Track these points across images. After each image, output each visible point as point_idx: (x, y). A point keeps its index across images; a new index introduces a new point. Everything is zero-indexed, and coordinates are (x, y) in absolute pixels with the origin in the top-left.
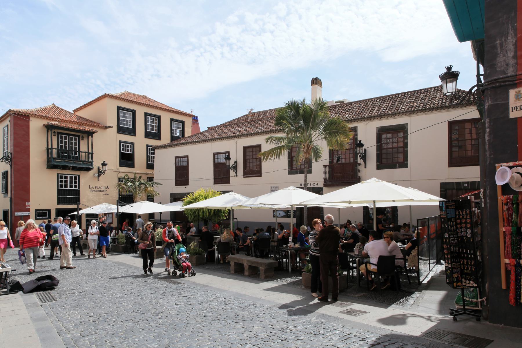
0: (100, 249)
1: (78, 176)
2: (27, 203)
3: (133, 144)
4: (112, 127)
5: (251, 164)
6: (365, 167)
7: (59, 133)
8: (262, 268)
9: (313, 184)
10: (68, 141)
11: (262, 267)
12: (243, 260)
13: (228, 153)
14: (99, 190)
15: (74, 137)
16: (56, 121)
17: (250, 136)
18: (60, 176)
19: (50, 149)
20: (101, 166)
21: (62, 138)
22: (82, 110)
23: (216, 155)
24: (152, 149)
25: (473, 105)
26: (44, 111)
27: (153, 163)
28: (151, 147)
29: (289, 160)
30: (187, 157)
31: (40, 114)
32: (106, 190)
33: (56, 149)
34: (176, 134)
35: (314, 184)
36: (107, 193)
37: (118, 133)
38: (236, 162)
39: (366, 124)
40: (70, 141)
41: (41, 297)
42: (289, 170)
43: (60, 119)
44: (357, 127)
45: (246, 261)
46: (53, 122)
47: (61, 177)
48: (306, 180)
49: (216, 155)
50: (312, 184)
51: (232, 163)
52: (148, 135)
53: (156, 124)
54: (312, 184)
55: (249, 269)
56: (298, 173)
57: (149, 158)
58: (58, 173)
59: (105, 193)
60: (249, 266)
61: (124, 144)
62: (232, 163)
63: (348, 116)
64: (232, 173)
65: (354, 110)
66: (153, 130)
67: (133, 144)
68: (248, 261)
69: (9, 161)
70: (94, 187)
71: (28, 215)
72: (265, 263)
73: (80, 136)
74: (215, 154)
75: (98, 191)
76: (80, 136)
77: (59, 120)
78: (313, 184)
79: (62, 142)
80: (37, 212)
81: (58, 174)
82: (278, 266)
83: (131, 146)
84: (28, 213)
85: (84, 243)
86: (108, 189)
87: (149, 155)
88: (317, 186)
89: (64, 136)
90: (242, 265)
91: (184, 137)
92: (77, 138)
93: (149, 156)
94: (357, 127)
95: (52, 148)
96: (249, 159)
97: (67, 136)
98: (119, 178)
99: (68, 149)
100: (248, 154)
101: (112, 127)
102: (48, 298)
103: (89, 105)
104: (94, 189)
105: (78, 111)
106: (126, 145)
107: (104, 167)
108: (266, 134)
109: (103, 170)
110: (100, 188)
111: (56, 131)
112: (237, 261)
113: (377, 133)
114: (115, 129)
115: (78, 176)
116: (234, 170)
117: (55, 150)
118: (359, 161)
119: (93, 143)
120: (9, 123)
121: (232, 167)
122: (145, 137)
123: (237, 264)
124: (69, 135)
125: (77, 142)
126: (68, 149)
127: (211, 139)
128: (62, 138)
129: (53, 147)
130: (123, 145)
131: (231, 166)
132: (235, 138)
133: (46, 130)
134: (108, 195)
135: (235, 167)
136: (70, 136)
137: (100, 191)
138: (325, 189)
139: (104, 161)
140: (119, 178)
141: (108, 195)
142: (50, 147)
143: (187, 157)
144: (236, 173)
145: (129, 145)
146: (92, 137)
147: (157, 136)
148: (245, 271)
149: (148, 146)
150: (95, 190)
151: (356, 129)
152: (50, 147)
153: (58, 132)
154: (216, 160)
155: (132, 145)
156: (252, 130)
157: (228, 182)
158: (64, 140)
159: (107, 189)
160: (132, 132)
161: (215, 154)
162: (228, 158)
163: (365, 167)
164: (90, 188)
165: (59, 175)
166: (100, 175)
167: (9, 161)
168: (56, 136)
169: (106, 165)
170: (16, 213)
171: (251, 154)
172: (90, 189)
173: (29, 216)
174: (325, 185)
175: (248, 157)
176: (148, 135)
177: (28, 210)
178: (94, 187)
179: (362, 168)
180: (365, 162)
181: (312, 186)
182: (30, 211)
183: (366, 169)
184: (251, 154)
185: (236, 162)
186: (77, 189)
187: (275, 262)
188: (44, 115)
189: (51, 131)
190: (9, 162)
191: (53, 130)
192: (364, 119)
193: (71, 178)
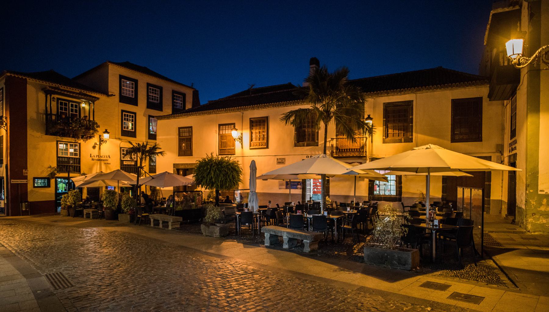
2: (24, 170)
3: (135, 114)
4: (115, 95)
7: (58, 99)
12: (281, 232)
15: (74, 104)
19: (49, 114)
25: (474, 85)
30: (191, 127)
32: (107, 159)
34: (128, 128)
41: (52, 280)
42: (296, 142)
45: (285, 233)
53: (158, 94)
55: (288, 242)
60: (289, 238)
61: (126, 113)
66: (127, 115)
67: (135, 114)
68: (288, 233)
69: (4, 125)
70: (95, 156)
71: (25, 182)
79: (61, 109)
80: (266, 118)
82: (119, 214)
84: (25, 180)
85: (87, 212)
89: (64, 102)
97: (67, 102)
98: (121, 148)
99: (68, 116)
101: (115, 95)
102: (62, 282)
106: (125, 114)
113: (384, 109)
120: (4, 86)
123: (155, 220)
124: (69, 101)
126: (68, 116)
130: (125, 115)
136: (70, 103)
140: (121, 148)
143: (191, 127)
145: (131, 115)
153: (57, 98)
155: (134, 115)
160: (134, 101)
164: (91, 157)
165: (122, 149)
166: (102, 144)
167: (4, 125)
172: (91, 158)
173: (27, 184)
177: (26, 178)
178: (95, 156)
186: (78, 157)
189: (51, 96)
190: (4, 127)
191: (53, 96)
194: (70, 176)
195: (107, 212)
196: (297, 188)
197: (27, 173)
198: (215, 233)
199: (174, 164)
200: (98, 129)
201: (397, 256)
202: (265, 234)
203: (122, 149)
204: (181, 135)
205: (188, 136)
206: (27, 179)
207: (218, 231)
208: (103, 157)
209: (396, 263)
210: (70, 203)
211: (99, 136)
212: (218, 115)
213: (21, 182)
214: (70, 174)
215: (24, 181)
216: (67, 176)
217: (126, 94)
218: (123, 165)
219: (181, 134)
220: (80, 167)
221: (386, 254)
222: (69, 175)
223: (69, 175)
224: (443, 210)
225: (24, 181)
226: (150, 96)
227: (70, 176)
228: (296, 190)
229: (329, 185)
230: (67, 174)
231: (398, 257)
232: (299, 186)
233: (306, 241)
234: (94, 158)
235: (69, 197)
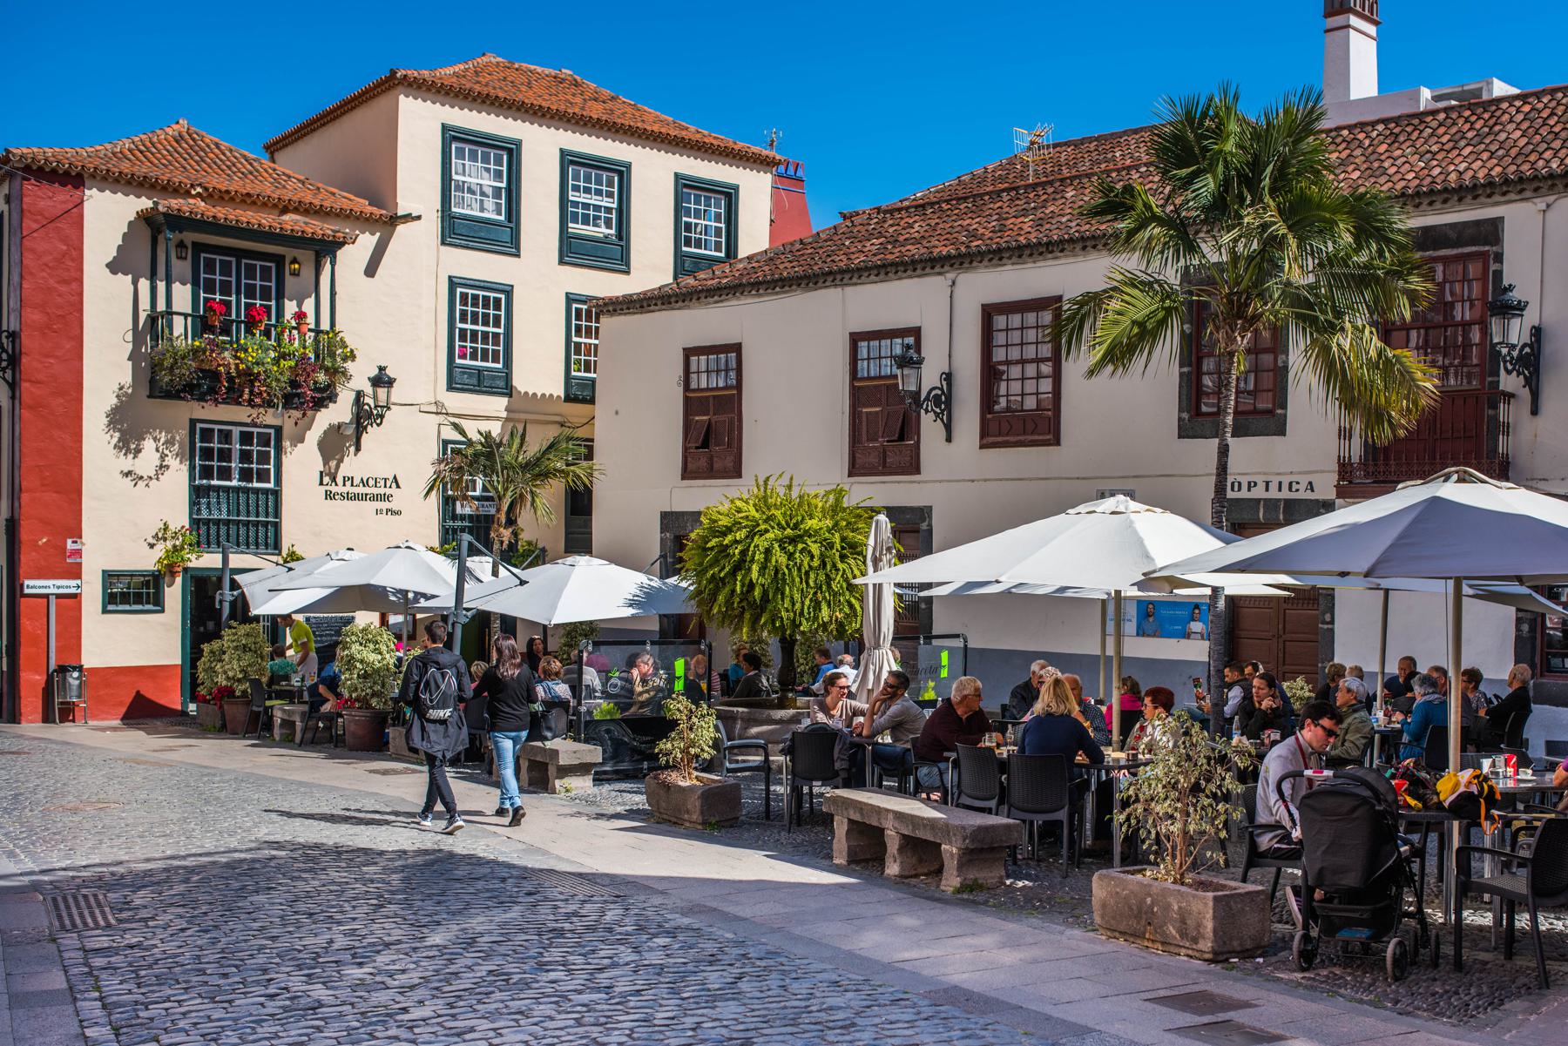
0: (300, 745)
1: (272, 431)
2: (69, 541)
4: (419, 218)
5: (1016, 387)
6: (1535, 411)
7: (199, 248)
8: (950, 849)
9: (1291, 484)
10: (233, 279)
11: (950, 843)
13: (916, 332)
14: (361, 490)
15: (258, 263)
16: (188, 194)
17: (1014, 259)
18: (201, 429)
20: (368, 389)
21: (210, 267)
22: (300, 142)
23: (863, 345)
24: (589, 312)
26: (141, 152)
27: (592, 375)
28: (584, 302)
29: (1185, 370)
30: (737, 348)
31: (125, 167)
32: (388, 491)
33: (186, 316)
35: (1295, 487)
36: (393, 505)
37: (443, 243)
38: (948, 377)
39: (1543, 206)
40: (243, 281)
42: (1185, 415)
43: (206, 189)
44: (1502, 218)
45: (891, 816)
46: (175, 203)
47: (207, 435)
48: (1222, 469)
49: (863, 345)
50: (1285, 487)
51: (930, 377)
52: (572, 250)
53: (610, 195)
54: (1285, 487)
55: (901, 850)
56: (1495, 379)
57: (578, 352)
58: (196, 416)
59: (384, 505)
60: (904, 836)
62: (930, 377)
63: (1467, 169)
64: (929, 426)
65: (1503, 136)
71: (73, 591)
72: (963, 828)
73: (283, 257)
74: (855, 339)
75: (356, 497)
76: (283, 257)
77: (199, 190)
78: (1291, 484)
81: (193, 422)
83: (497, 301)
86: (398, 487)
87: (575, 339)
88: (1309, 496)
90: (880, 831)
91: (735, 256)
92: (273, 265)
93: (578, 345)
94: (1502, 218)
95: (169, 313)
96: (1008, 363)
97: (233, 260)
100: (1000, 338)
101: (419, 218)
103: (290, 144)
104: (340, 489)
105: (286, 146)
107: (382, 392)
108: (1084, 248)
109: (376, 407)
110: (365, 483)
111: (190, 237)
112: (857, 817)
114: (431, 224)
115: (272, 431)
116: (937, 415)
117: (182, 318)
118: (1510, 382)
119: (338, 289)
121: (927, 398)
122: (561, 262)
123: (857, 828)
124: (240, 254)
125: (273, 285)
127: (842, 272)
128: (210, 267)
129: (175, 309)
130: (464, 297)
131: (923, 396)
132: (947, 268)
133: (146, 233)
134: (398, 513)
135: (944, 401)
136: (244, 261)
137: (363, 497)
138: (1338, 501)
139: (382, 369)
141: (398, 513)
142: (161, 307)
143: (737, 348)
144: (948, 427)
146: (333, 265)
147: (615, 255)
148: (889, 861)
149: (570, 299)
150: (345, 490)
151: (1496, 228)
152: (161, 307)
153: (194, 244)
154: (862, 365)
156: (1025, 229)
157: (914, 468)
158: (218, 277)
159: (394, 490)
161: (855, 339)
162: (910, 360)
163: (1535, 411)
164: (321, 484)
165: (199, 426)
166: (365, 428)
168: (186, 258)
169: (390, 383)
170: (27, 582)
171: (1015, 337)
172: (324, 488)
174: (1339, 496)
175: (999, 355)
176: (572, 250)
177: (75, 572)
179: (1514, 413)
180: (1534, 385)
181: (1285, 494)
182: (84, 576)
183: (1540, 421)
184: (1015, 337)
185: (948, 377)
186: (271, 485)
187: (1008, 826)
188: (142, 169)
192: (1536, 184)
193: (246, 438)
194: (232, 565)
195: (350, 721)
196: (1187, 635)
197: (78, 553)
198: (688, 812)
199: (665, 516)
200: (349, 365)
201: (1176, 908)
202: (836, 818)
203: (199, 426)
204: (693, 385)
205: (722, 389)
206: (78, 576)
207: (698, 804)
208: (371, 482)
209: (1174, 932)
210: (228, 678)
211: (353, 395)
212: (849, 290)
213: (58, 587)
214: (231, 556)
215: (67, 585)
216: (220, 566)
217: (482, 209)
218: (454, 517)
219: (694, 377)
220: (277, 527)
221: (1149, 900)
222: (225, 560)
223: (225, 560)
224: (1321, 717)
225: (67, 585)
226: (576, 204)
227: (232, 565)
228: (1184, 642)
229: (1332, 622)
230: (220, 556)
231: (1180, 908)
232: (1197, 626)
233: (947, 847)
234: (334, 489)
235: (224, 653)
